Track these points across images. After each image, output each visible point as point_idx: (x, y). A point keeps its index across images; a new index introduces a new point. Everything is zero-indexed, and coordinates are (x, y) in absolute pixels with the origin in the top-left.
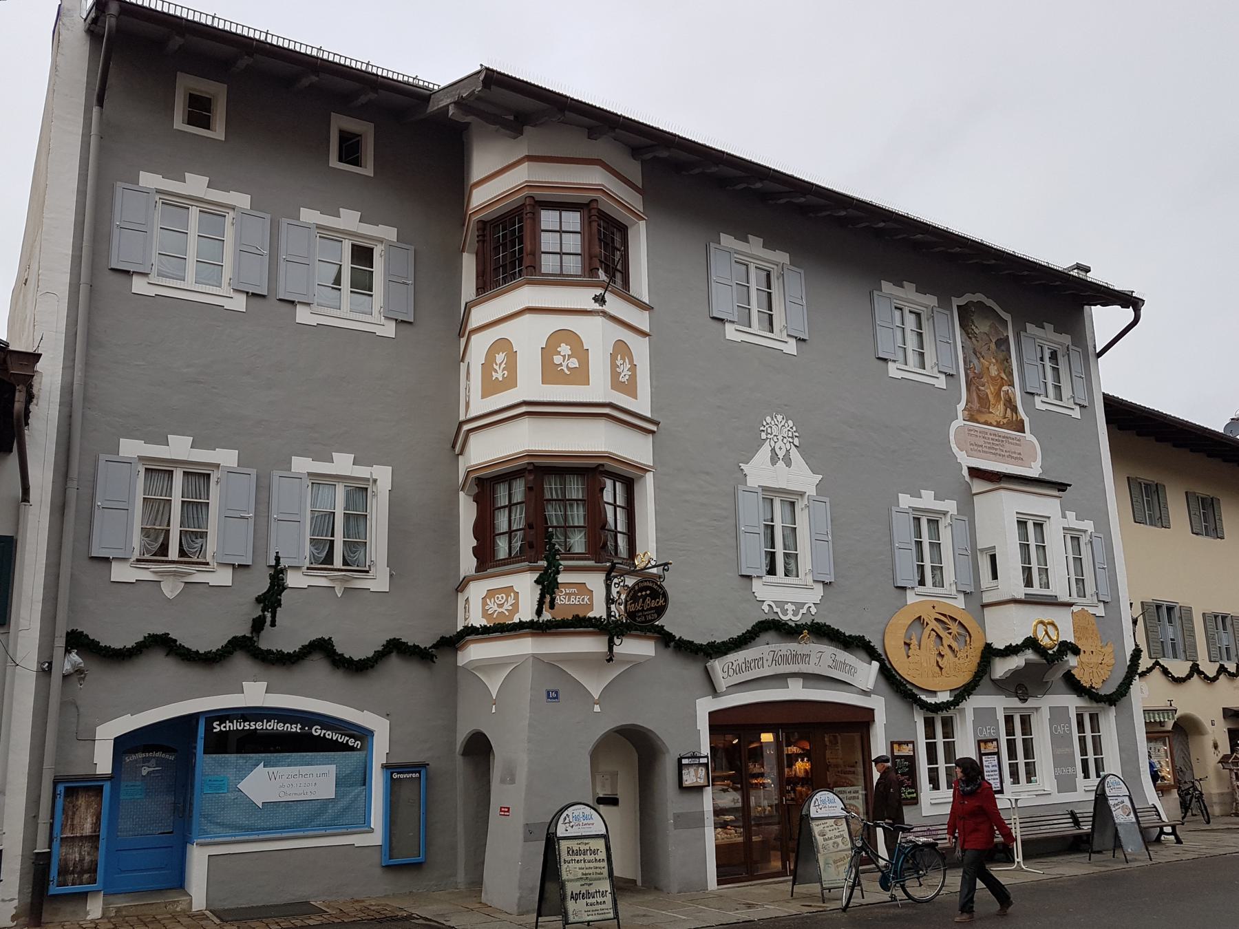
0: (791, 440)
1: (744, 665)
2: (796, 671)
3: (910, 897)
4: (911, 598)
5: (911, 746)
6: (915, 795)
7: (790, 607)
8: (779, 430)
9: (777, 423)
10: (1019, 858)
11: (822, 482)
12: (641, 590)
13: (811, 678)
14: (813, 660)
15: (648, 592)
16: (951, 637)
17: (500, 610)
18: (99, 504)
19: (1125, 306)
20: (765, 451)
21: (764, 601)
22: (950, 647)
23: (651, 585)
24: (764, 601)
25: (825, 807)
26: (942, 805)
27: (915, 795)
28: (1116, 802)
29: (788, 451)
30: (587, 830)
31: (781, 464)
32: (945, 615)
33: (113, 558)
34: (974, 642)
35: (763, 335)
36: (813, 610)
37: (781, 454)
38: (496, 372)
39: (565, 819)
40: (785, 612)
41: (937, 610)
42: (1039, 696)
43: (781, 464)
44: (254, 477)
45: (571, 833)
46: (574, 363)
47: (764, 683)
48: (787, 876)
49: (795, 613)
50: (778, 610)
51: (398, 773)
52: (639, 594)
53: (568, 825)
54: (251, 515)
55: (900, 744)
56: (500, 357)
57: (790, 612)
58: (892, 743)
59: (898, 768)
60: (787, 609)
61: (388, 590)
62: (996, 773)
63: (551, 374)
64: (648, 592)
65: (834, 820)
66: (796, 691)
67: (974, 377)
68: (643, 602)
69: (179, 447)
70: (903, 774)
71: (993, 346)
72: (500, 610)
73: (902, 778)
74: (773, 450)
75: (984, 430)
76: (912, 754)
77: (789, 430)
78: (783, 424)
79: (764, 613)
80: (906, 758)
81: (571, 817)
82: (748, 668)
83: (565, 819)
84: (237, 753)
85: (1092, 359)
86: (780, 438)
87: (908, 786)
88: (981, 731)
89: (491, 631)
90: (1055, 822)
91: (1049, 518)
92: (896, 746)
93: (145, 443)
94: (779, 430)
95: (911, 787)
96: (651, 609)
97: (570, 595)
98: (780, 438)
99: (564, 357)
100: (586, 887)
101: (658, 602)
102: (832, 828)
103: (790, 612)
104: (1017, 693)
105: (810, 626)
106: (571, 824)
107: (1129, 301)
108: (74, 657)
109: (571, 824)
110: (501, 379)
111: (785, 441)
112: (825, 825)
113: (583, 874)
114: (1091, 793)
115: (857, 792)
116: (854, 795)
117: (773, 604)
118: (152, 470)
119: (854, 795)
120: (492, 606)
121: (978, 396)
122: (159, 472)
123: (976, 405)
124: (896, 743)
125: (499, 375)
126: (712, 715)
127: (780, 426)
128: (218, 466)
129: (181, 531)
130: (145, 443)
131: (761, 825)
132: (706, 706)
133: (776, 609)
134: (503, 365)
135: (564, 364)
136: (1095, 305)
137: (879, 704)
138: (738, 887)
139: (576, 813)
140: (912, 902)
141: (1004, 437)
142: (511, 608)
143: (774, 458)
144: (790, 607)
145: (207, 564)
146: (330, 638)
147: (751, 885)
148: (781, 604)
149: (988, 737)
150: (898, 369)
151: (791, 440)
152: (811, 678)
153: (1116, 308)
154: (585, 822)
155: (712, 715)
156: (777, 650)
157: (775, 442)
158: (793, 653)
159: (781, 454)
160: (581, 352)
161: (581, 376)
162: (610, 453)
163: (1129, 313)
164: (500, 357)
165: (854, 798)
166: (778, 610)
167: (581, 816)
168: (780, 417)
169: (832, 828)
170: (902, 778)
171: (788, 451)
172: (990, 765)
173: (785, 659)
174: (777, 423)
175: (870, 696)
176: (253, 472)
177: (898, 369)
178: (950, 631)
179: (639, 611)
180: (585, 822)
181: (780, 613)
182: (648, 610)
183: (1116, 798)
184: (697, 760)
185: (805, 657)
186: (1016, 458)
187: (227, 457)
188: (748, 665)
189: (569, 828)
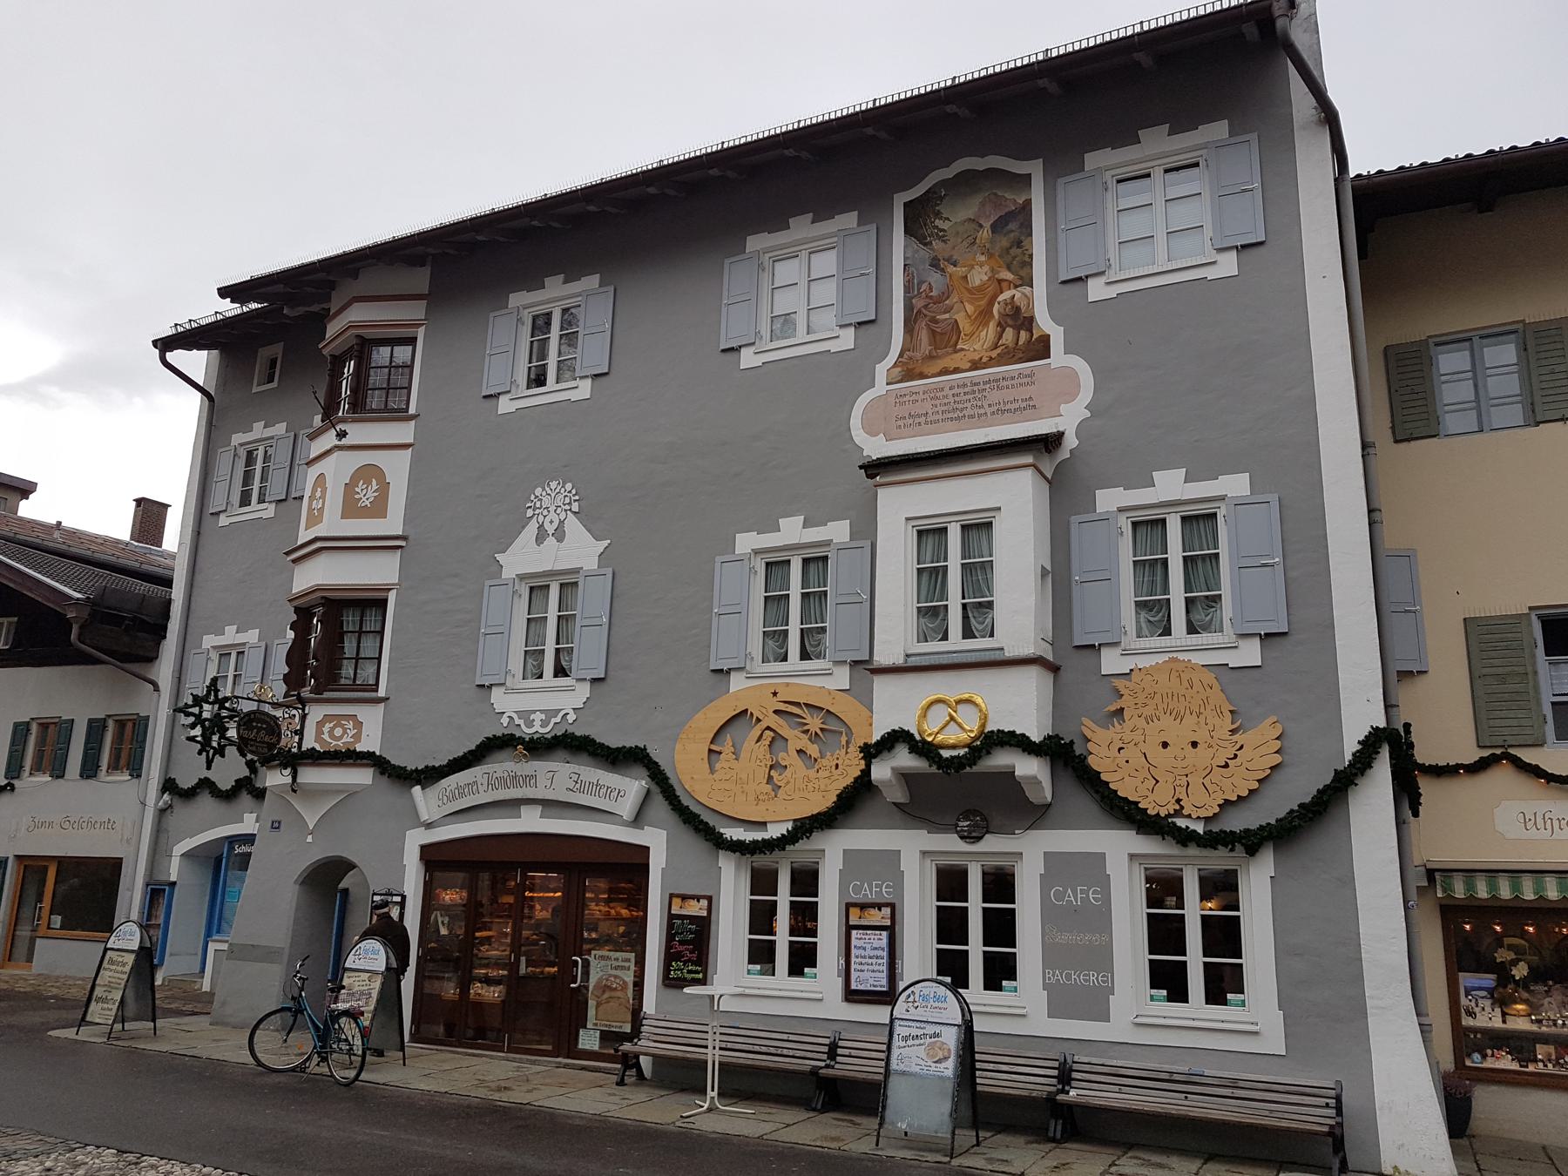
0: (567, 507)
1: (457, 791)
2: (520, 797)
3: (259, 1063)
4: (737, 683)
5: (887, 911)
6: (701, 976)
7: (538, 717)
8: (553, 501)
9: (549, 492)
10: (712, 1094)
11: (608, 549)
13: (550, 806)
14: (542, 781)
16: (805, 737)
18: (1077, 578)
20: (532, 528)
21: (504, 713)
22: (800, 752)
23: (269, 720)
24: (504, 713)
25: (366, 958)
26: (754, 999)
27: (701, 976)
28: (919, 1032)
29: (562, 522)
30: (934, 1014)
31: (551, 541)
32: (797, 704)
33: (1100, 645)
34: (1274, 728)
35: (563, 388)
36: (571, 718)
37: (550, 529)
39: (909, 996)
40: (530, 724)
41: (780, 697)
42: (1017, 832)
43: (551, 541)
44: (1275, 505)
45: (914, 1014)
47: (487, 812)
48: (504, 1052)
49: (544, 724)
50: (521, 722)
53: (911, 1004)
54: (1277, 560)
55: (684, 898)
57: (537, 724)
58: (672, 896)
59: (677, 933)
60: (534, 720)
61: (848, 688)
62: (881, 961)
63: (351, 508)
65: (369, 974)
66: (531, 822)
67: (926, 307)
68: (257, 733)
69: (1170, 485)
70: (681, 943)
71: (985, 234)
72: (340, 739)
73: (681, 948)
74: (541, 526)
75: (933, 386)
76: (705, 914)
77: (566, 496)
78: (557, 490)
79: (501, 727)
80: (692, 919)
81: (917, 995)
82: (462, 795)
83: (909, 996)
84: (1237, 890)
86: (552, 509)
87: (689, 961)
88: (857, 890)
89: (591, 749)
90: (991, 1066)
91: (999, 509)
92: (676, 902)
93: (1125, 489)
94: (553, 501)
95: (694, 963)
97: (260, 729)
98: (552, 509)
99: (367, 495)
100: (107, 994)
101: (271, 739)
102: (364, 983)
103: (537, 724)
104: (957, 826)
105: (528, 742)
106: (916, 1005)
108: (166, 797)
109: (916, 1005)
111: (559, 510)
112: (357, 979)
113: (109, 982)
114: (101, 943)
115: (629, 960)
116: (623, 964)
117: (515, 716)
118: (1197, 517)
119: (623, 964)
121: (933, 333)
122: (1149, 527)
123: (925, 346)
124: (678, 896)
126: (425, 849)
127: (553, 495)
128: (1222, 498)
129: (802, 630)
130: (1125, 489)
132: (415, 840)
133: (517, 721)
137: (656, 840)
138: (422, 1048)
139: (926, 991)
140: (263, 1070)
141: (985, 383)
143: (541, 537)
144: (538, 717)
146: (1372, 727)
147: (437, 1050)
148: (525, 715)
149: (872, 897)
150: (756, 353)
151: (567, 507)
152: (550, 806)
154: (936, 1004)
155: (425, 849)
156: (491, 771)
157: (545, 517)
158: (511, 774)
159: (550, 529)
161: (379, 509)
162: (318, 585)
165: (623, 968)
166: (521, 722)
167: (932, 996)
169: (364, 983)
170: (681, 948)
171: (562, 522)
172: (868, 946)
173: (503, 782)
174: (549, 492)
175: (643, 829)
176: (1273, 498)
177: (756, 353)
178: (806, 728)
180: (936, 1004)
181: (523, 726)
183: (922, 1025)
184: (390, 898)
185: (530, 779)
186: (958, 419)
187: (1236, 485)
188: (461, 792)
189: (912, 1010)
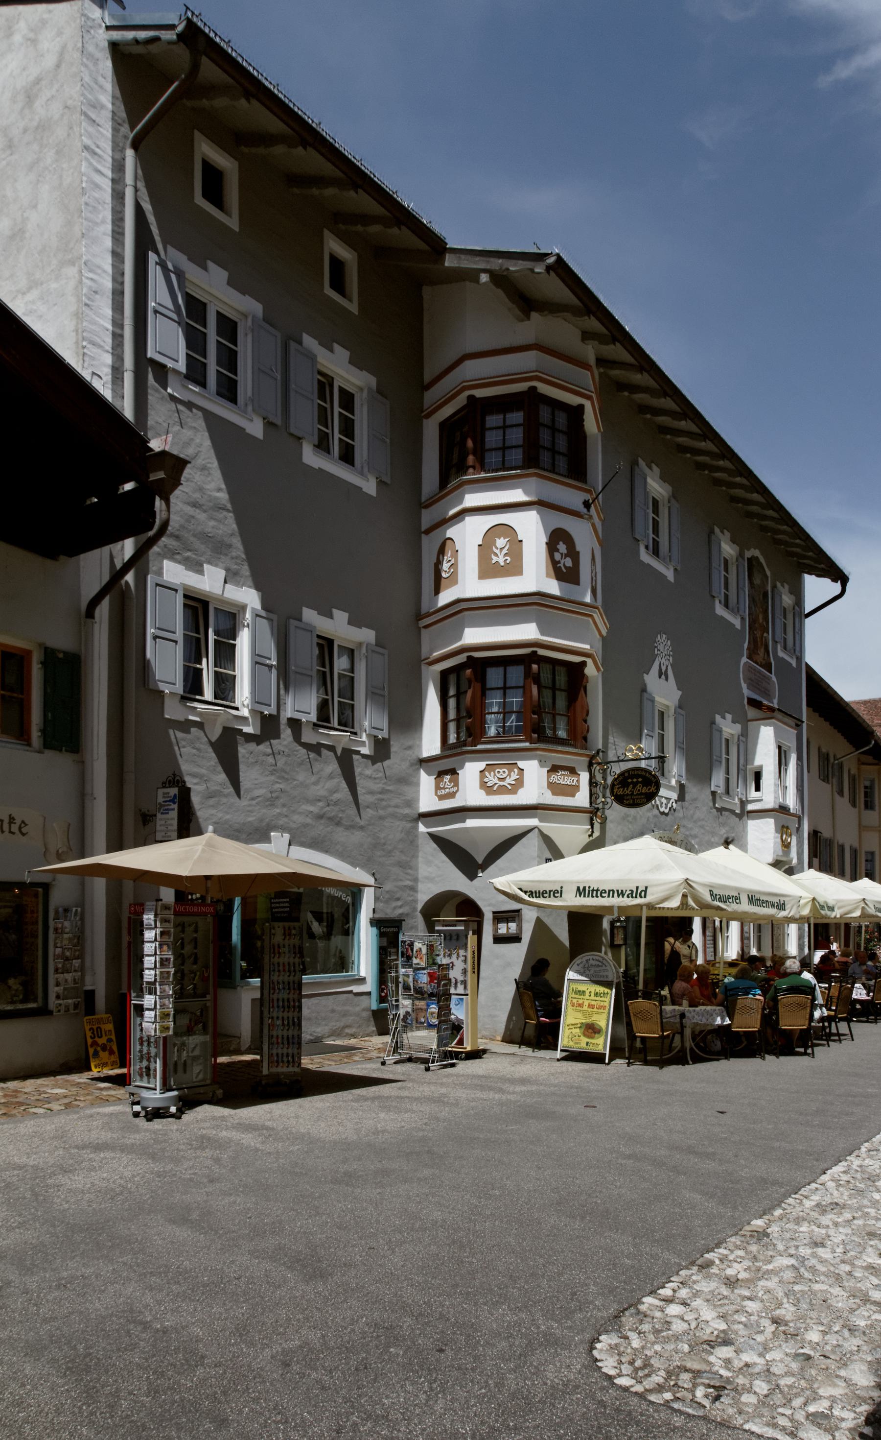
12: (632, 777)
15: (640, 780)
17: (502, 783)
19: (835, 580)
38: (496, 555)
46: (569, 562)
51: (385, 927)
52: (630, 780)
56: (562, 547)
64: (640, 780)
85: (803, 617)
96: (642, 794)
107: (841, 577)
110: (502, 564)
120: (491, 778)
125: (501, 559)
131: (141, 1044)
134: (505, 551)
135: (562, 562)
136: (811, 574)
142: (514, 782)
145: (237, 709)
153: (826, 581)
160: (516, 545)
161: (514, 568)
163: (837, 588)
164: (501, 542)
168: (664, 636)
179: (628, 795)
182: (637, 794)
